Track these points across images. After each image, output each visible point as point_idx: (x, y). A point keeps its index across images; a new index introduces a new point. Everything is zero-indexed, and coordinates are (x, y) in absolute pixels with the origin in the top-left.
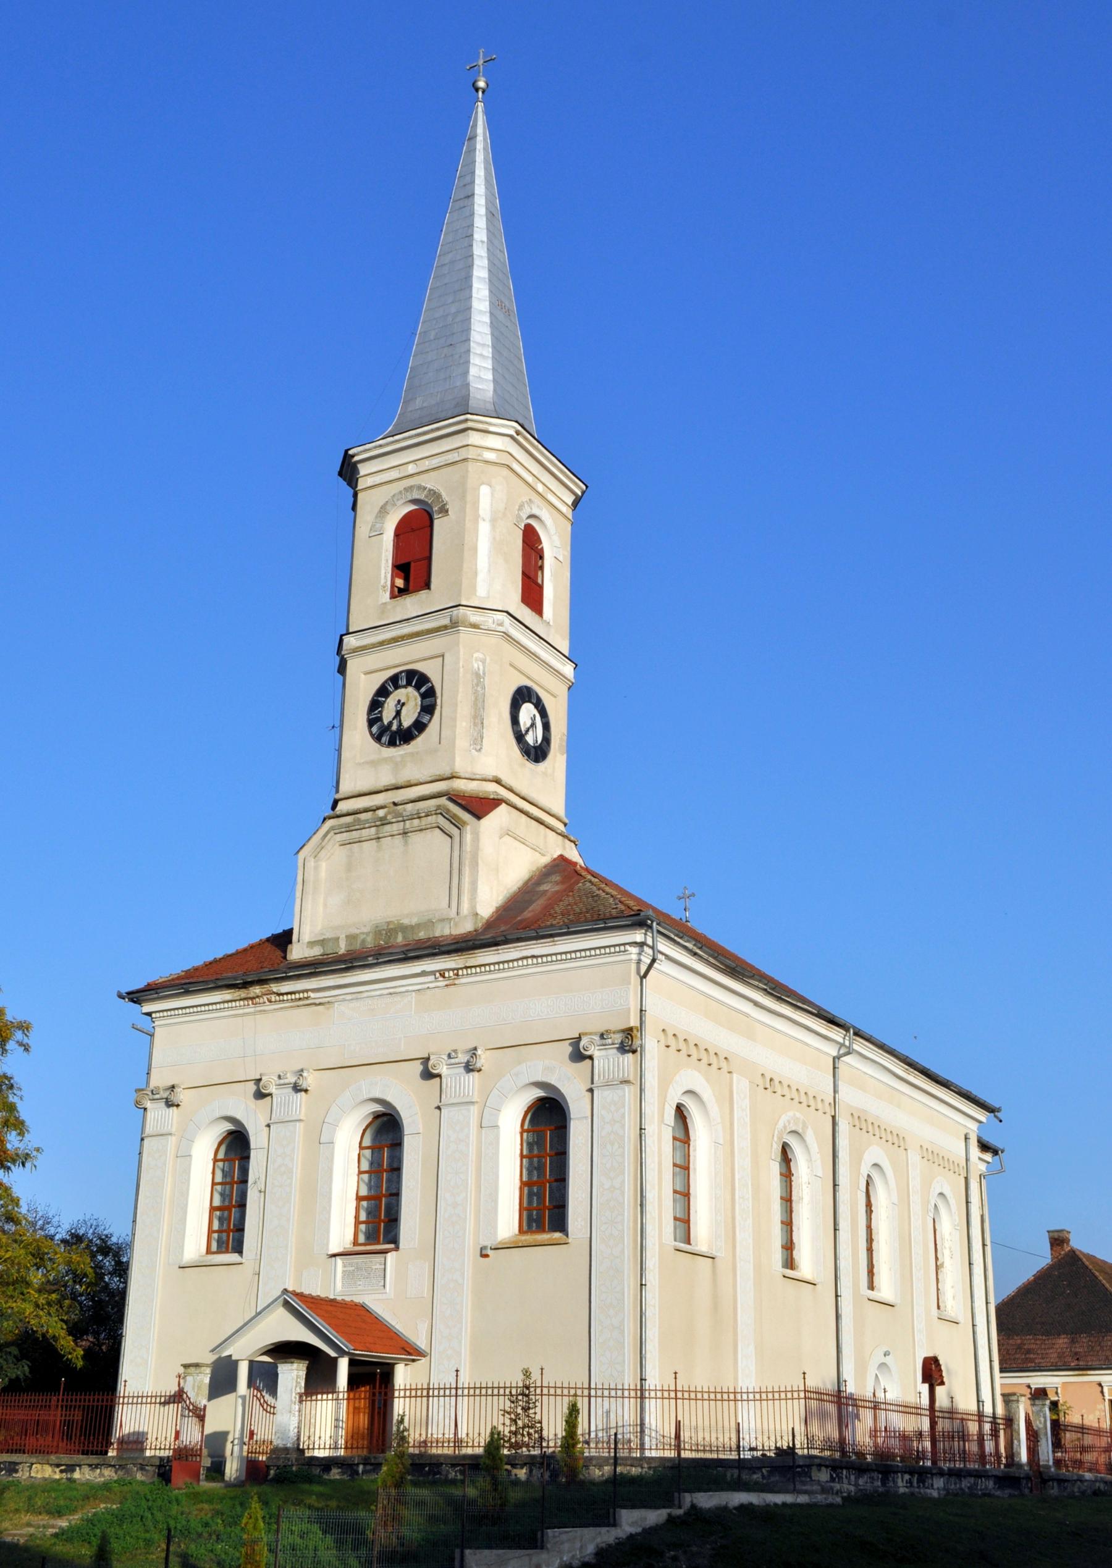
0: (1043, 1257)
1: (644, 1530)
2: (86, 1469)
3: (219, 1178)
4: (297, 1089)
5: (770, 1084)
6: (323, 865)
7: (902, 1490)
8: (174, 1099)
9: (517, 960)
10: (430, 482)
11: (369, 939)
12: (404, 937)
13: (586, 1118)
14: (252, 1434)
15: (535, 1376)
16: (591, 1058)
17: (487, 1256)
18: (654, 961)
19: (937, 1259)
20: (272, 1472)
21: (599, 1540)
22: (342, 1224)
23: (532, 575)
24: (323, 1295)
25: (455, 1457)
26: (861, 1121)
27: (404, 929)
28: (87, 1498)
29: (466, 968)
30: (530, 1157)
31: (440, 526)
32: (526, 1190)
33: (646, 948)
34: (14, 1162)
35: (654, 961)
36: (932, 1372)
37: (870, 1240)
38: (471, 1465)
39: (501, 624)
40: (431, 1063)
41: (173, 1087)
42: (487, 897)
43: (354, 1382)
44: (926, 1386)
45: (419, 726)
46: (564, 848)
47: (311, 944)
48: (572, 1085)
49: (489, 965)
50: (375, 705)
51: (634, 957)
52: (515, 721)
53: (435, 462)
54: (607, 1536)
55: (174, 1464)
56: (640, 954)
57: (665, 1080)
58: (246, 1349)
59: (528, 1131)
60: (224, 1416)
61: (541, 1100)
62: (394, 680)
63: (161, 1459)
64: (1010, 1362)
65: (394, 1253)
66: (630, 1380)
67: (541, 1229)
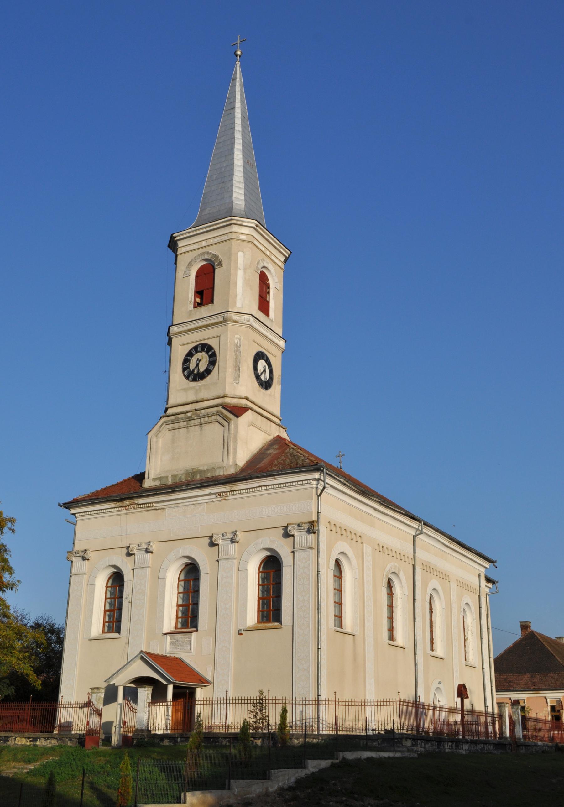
0: (517, 635)
1: (319, 770)
2: (43, 740)
3: (109, 596)
4: (147, 551)
5: (382, 549)
6: (160, 440)
7: (447, 750)
8: (86, 556)
9: (256, 487)
10: (213, 250)
11: (183, 477)
12: (200, 476)
13: (291, 566)
14: (125, 722)
15: (266, 693)
16: (293, 536)
17: (241, 634)
18: (324, 488)
19: (465, 635)
20: (135, 741)
21: (297, 775)
22: (170, 619)
23: (264, 297)
24: (160, 654)
25: (226, 734)
26: (427, 567)
27: (200, 472)
28: (43, 754)
29: (231, 491)
30: (263, 585)
31: (218, 272)
32: (261, 601)
33: (320, 481)
34: (7, 587)
35: (324, 488)
36: (462, 692)
37: (431, 626)
38: (234, 738)
39: (249, 321)
40: (214, 538)
41: (86, 550)
42: (242, 456)
43: (176, 696)
44: (459, 699)
45: (208, 372)
46: (280, 432)
47: (154, 479)
48: (283, 550)
49: (243, 490)
50: (186, 361)
51: (315, 486)
52: (255, 368)
53: (216, 240)
54: (301, 773)
55: (87, 737)
56: (317, 484)
57: (330, 546)
58: (122, 681)
59: (262, 572)
60: (111, 713)
61: (268, 557)
62: (196, 349)
63: (80, 735)
64: (501, 687)
65: (195, 633)
66: (312, 696)
67: (268, 621)
